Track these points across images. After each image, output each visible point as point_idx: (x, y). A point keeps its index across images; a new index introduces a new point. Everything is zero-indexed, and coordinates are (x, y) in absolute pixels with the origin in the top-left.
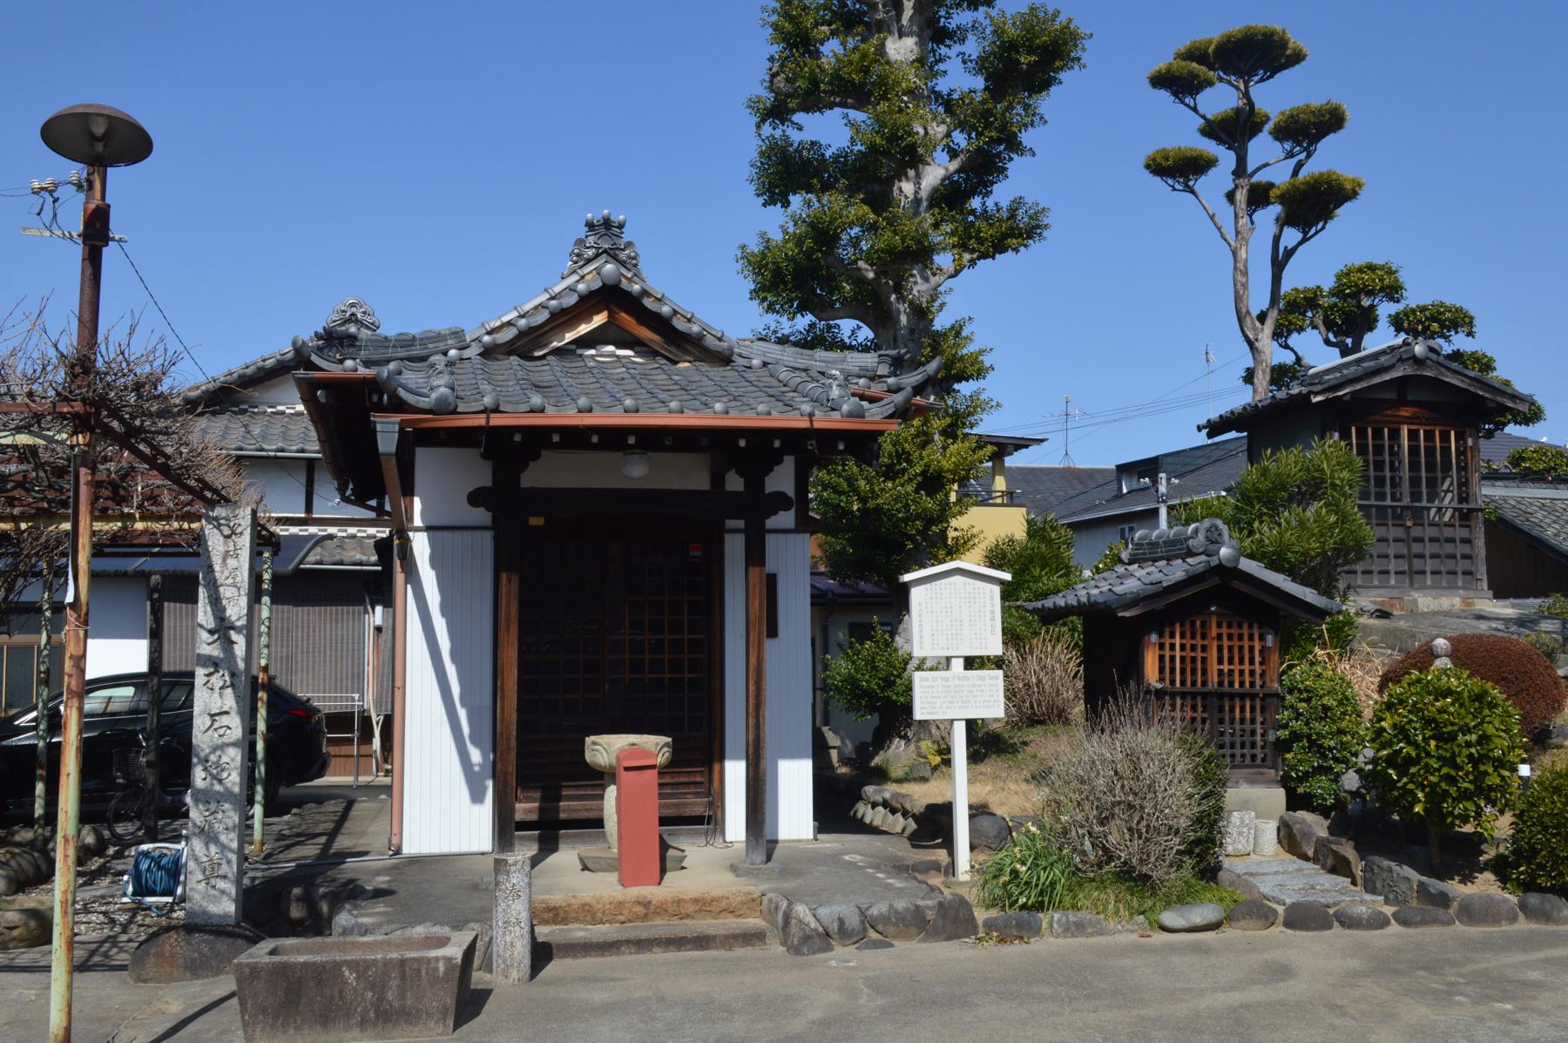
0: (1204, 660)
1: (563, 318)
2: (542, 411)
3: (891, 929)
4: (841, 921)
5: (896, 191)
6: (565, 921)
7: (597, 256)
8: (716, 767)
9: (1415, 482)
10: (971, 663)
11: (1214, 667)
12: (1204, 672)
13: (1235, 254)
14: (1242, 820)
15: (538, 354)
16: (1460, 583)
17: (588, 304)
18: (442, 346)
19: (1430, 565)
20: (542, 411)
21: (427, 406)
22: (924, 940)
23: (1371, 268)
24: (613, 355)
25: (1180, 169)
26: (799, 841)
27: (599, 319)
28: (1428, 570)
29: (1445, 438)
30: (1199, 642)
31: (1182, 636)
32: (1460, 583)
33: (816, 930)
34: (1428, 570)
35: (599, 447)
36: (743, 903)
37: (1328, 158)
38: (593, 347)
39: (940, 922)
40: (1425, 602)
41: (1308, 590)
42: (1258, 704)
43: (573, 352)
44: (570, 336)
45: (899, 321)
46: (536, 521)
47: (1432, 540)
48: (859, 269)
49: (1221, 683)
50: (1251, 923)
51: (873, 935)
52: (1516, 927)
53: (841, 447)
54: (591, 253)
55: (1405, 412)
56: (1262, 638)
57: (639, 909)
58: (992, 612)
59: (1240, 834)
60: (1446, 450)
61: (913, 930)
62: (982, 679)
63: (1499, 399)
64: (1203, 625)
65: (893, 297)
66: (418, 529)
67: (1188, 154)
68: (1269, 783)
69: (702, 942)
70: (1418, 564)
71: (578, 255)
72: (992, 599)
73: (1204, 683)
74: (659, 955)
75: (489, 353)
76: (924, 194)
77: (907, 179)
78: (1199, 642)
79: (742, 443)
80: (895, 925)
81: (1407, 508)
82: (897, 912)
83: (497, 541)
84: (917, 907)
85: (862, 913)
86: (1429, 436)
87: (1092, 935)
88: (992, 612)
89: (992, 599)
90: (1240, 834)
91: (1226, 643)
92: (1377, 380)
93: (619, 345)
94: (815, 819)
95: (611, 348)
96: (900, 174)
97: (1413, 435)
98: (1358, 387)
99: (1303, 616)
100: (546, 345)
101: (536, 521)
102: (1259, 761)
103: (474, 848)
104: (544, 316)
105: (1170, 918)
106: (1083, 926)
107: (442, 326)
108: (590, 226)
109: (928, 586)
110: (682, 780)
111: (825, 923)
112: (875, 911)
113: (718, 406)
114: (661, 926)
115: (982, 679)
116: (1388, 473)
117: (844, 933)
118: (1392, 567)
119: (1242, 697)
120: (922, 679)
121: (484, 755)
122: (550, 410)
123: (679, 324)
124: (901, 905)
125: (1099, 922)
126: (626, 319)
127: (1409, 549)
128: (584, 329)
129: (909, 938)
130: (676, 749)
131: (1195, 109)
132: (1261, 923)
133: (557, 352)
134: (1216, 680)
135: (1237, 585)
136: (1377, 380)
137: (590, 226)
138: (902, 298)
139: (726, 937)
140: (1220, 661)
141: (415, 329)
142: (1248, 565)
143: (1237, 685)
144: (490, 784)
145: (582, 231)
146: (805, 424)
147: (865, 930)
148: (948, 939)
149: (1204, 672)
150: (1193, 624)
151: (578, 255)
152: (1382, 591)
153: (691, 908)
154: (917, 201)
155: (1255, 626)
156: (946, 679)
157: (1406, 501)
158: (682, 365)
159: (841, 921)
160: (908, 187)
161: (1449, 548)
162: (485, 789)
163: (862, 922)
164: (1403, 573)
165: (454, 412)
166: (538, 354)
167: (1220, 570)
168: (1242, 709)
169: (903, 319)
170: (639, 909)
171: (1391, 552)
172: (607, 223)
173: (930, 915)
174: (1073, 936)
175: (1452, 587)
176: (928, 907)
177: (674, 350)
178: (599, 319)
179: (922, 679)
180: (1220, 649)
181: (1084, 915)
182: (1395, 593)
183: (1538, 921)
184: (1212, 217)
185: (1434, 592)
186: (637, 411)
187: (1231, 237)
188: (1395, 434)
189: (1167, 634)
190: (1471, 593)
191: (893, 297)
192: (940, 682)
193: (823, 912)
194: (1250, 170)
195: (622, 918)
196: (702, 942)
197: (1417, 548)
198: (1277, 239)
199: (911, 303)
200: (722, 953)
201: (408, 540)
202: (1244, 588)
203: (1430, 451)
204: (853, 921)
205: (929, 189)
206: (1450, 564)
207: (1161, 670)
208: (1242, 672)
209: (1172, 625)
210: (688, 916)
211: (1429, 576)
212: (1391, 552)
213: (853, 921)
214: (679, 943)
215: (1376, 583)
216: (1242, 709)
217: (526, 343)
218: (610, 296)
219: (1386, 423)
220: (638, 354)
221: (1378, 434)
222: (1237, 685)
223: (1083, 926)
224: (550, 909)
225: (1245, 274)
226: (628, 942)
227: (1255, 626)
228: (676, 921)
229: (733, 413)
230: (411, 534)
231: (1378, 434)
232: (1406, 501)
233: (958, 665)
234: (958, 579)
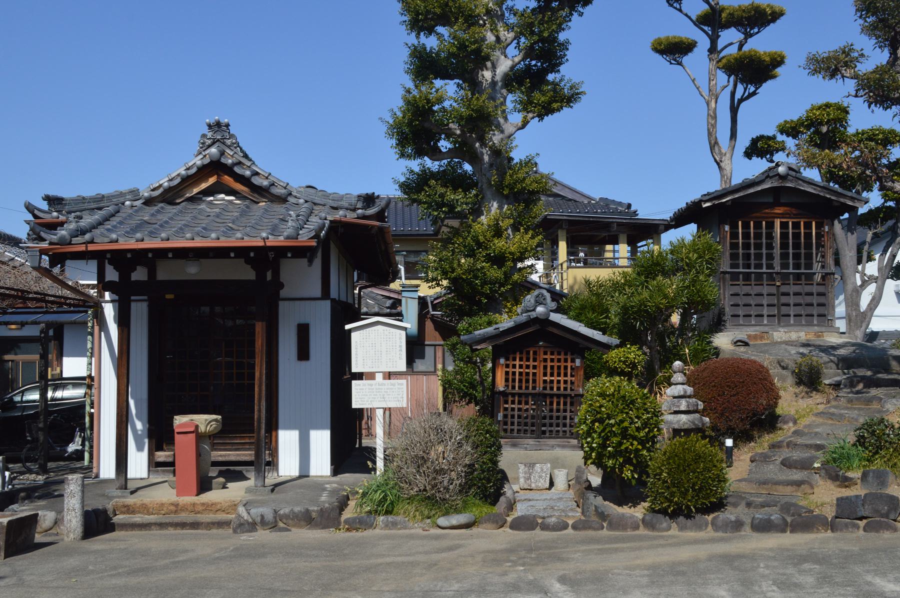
0: (534, 374)
1: (188, 181)
2: (117, 241)
3: (290, 522)
4: (262, 516)
5: (480, 78)
6: (133, 512)
7: (213, 143)
8: (274, 434)
9: (784, 256)
10: (389, 375)
11: (541, 378)
12: (534, 381)
13: (708, 104)
14: (542, 470)
15: (178, 201)
16: (815, 322)
17: (203, 172)
18: (122, 200)
19: (792, 311)
20: (117, 241)
21: (56, 241)
22: (309, 529)
23: (828, 105)
24: (223, 200)
25: (674, 50)
26: (322, 477)
27: (212, 180)
28: (792, 314)
29: (808, 226)
30: (531, 363)
31: (521, 360)
32: (815, 322)
33: (247, 521)
34: (792, 314)
35: (174, 257)
36: (229, 506)
37: (762, 43)
38: (212, 195)
39: (319, 520)
40: (780, 334)
41: (595, 332)
42: (569, 400)
43: (200, 199)
44: (196, 190)
45: (483, 159)
46: (169, 296)
47: (795, 294)
48: (450, 129)
49: (545, 388)
50: (489, 525)
51: (281, 525)
52: (637, 532)
53: (289, 255)
54: (209, 142)
55: (778, 210)
56: (573, 361)
57: (173, 508)
58: (400, 346)
59: (540, 477)
60: (808, 236)
61: (303, 523)
62: (394, 385)
63: (842, 200)
64: (535, 353)
65: (477, 145)
66: (107, 302)
67: (673, 41)
68: (573, 447)
69: (195, 525)
70: (784, 310)
71: (203, 143)
72: (400, 338)
73: (534, 388)
74: (171, 531)
75: (149, 202)
76: (498, 78)
77: (487, 69)
78: (531, 363)
79: (252, 254)
80: (292, 519)
81: (777, 273)
82: (294, 513)
83: (149, 306)
84: (307, 510)
85: (275, 512)
86: (796, 226)
87: (400, 529)
88: (400, 346)
89: (400, 338)
90: (540, 477)
91: (549, 364)
92: (751, 191)
93: (227, 194)
94: (332, 465)
95: (222, 196)
96: (483, 67)
97: (784, 226)
98: (737, 196)
99: (595, 348)
100: (183, 196)
101: (169, 296)
102: (568, 435)
103: (138, 476)
104: (178, 180)
105: (442, 521)
106: (396, 524)
107: (124, 187)
108: (210, 126)
109: (361, 331)
110: (248, 441)
111: (253, 516)
112: (282, 512)
113: (213, 235)
114: (184, 517)
115: (394, 385)
116: (764, 251)
117: (263, 522)
118: (765, 312)
119: (558, 396)
120: (356, 385)
121: (143, 425)
122: (121, 240)
123: (256, 181)
124: (297, 509)
125: (405, 522)
126: (228, 180)
127: (778, 300)
128: (204, 186)
129: (300, 527)
130: (224, 422)
131: (680, 10)
132: (494, 525)
133: (191, 199)
134: (542, 385)
135: (551, 329)
136: (751, 191)
137: (210, 126)
138: (483, 144)
139: (208, 523)
140: (545, 375)
141: (106, 190)
142: (555, 317)
143: (555, 389)
144: (146, 441)
145: (205, 130)
146: (261, 244)
147: (276, 521)
148: (323, 528)
149: (534, 381)
150: (528, 353)
151: (203, 143)
152: (758, 328)
153: (200, 508)
154: (494, 83)
155: (569, 353)
156: (371, 385)
157: (778, 269)
158: (261, 204)
159: (262, 516)
160: (488, 74)
161: (808, 299)
162: (144, 444)
163: (275, 517)
164: (774, 316)
165: (70, 244)
166: (178, 201)
167: (536, 320)
168: (558, 404)
169: (486, 158)
170: (173, 508)
171: (765, 302)
172: (218, 124)
173: (314, 515)
174: (390, 529)
175: (810, 324)
176: (313, 511)
177: (256, 195)
178: (212, 180)
179: (356, 385)
180: (545, 367)
181: (399, 518)
182: (766, 329)
183: (649, 530)
184: (693, 81)
185: (796, 328)
186: (168, 240)
187: (706, 93)
188: (771, 226)
189: (511, 359)
190: (823, 329)
191: (477, 145)
192: (397, 386)
193: (253, 511)
194: (719, 48)
195: (163, 512)
196: (195, 525)
197: (784, 300)
198: (733, 94)
199: (490, 147)
200: (205, 531)
201: (102, 308)
202: (555, 331)
203: (796, 236)
204: (269, 516)
205: (501, 74)
206: (809, 310)
207: (507, 380)
208: (559, 382)
209: (515, 353)
210: (199, 513)
211: (792, 318)
212: (765, 302)
213: (269, 516)
214: (183, 525)
215: (753, 322)
216: (558, 404)
217: (170, 196)
218: (215, 167)
219: (764, 218)
220: (238, 198)
221: (758, 226)
222: (555, 389)
223: (396, 524)
224: (125, 506)
225: (715, 118)
226: (155, 524)
227: (569, 353)
228: (192, 515)
229: (222, 239)
230: (103, 304)
231: (758, 226)
232: (778, 269)
233: (379, 377)
234: (379, 327)
